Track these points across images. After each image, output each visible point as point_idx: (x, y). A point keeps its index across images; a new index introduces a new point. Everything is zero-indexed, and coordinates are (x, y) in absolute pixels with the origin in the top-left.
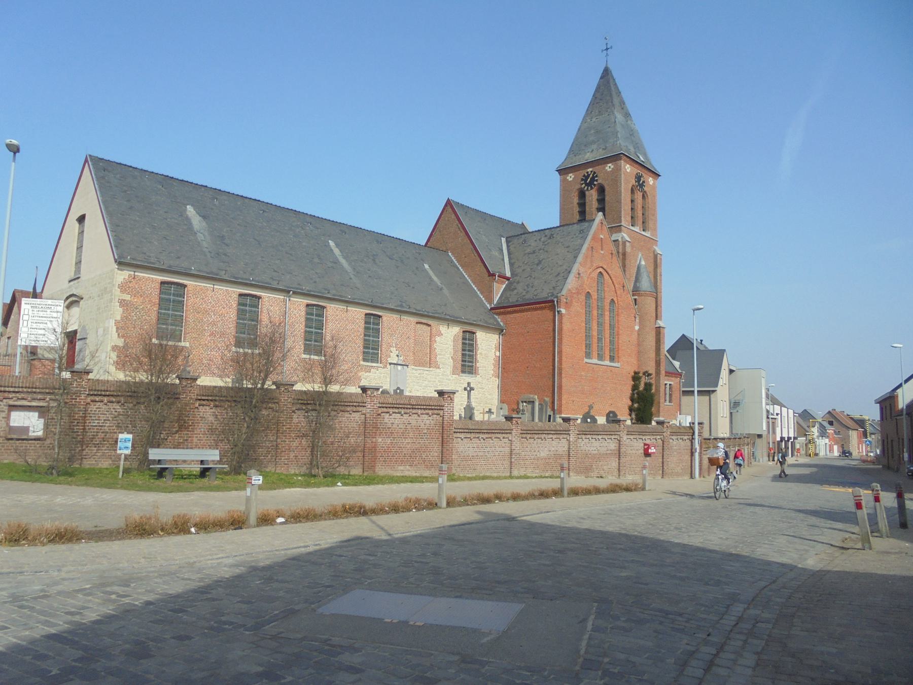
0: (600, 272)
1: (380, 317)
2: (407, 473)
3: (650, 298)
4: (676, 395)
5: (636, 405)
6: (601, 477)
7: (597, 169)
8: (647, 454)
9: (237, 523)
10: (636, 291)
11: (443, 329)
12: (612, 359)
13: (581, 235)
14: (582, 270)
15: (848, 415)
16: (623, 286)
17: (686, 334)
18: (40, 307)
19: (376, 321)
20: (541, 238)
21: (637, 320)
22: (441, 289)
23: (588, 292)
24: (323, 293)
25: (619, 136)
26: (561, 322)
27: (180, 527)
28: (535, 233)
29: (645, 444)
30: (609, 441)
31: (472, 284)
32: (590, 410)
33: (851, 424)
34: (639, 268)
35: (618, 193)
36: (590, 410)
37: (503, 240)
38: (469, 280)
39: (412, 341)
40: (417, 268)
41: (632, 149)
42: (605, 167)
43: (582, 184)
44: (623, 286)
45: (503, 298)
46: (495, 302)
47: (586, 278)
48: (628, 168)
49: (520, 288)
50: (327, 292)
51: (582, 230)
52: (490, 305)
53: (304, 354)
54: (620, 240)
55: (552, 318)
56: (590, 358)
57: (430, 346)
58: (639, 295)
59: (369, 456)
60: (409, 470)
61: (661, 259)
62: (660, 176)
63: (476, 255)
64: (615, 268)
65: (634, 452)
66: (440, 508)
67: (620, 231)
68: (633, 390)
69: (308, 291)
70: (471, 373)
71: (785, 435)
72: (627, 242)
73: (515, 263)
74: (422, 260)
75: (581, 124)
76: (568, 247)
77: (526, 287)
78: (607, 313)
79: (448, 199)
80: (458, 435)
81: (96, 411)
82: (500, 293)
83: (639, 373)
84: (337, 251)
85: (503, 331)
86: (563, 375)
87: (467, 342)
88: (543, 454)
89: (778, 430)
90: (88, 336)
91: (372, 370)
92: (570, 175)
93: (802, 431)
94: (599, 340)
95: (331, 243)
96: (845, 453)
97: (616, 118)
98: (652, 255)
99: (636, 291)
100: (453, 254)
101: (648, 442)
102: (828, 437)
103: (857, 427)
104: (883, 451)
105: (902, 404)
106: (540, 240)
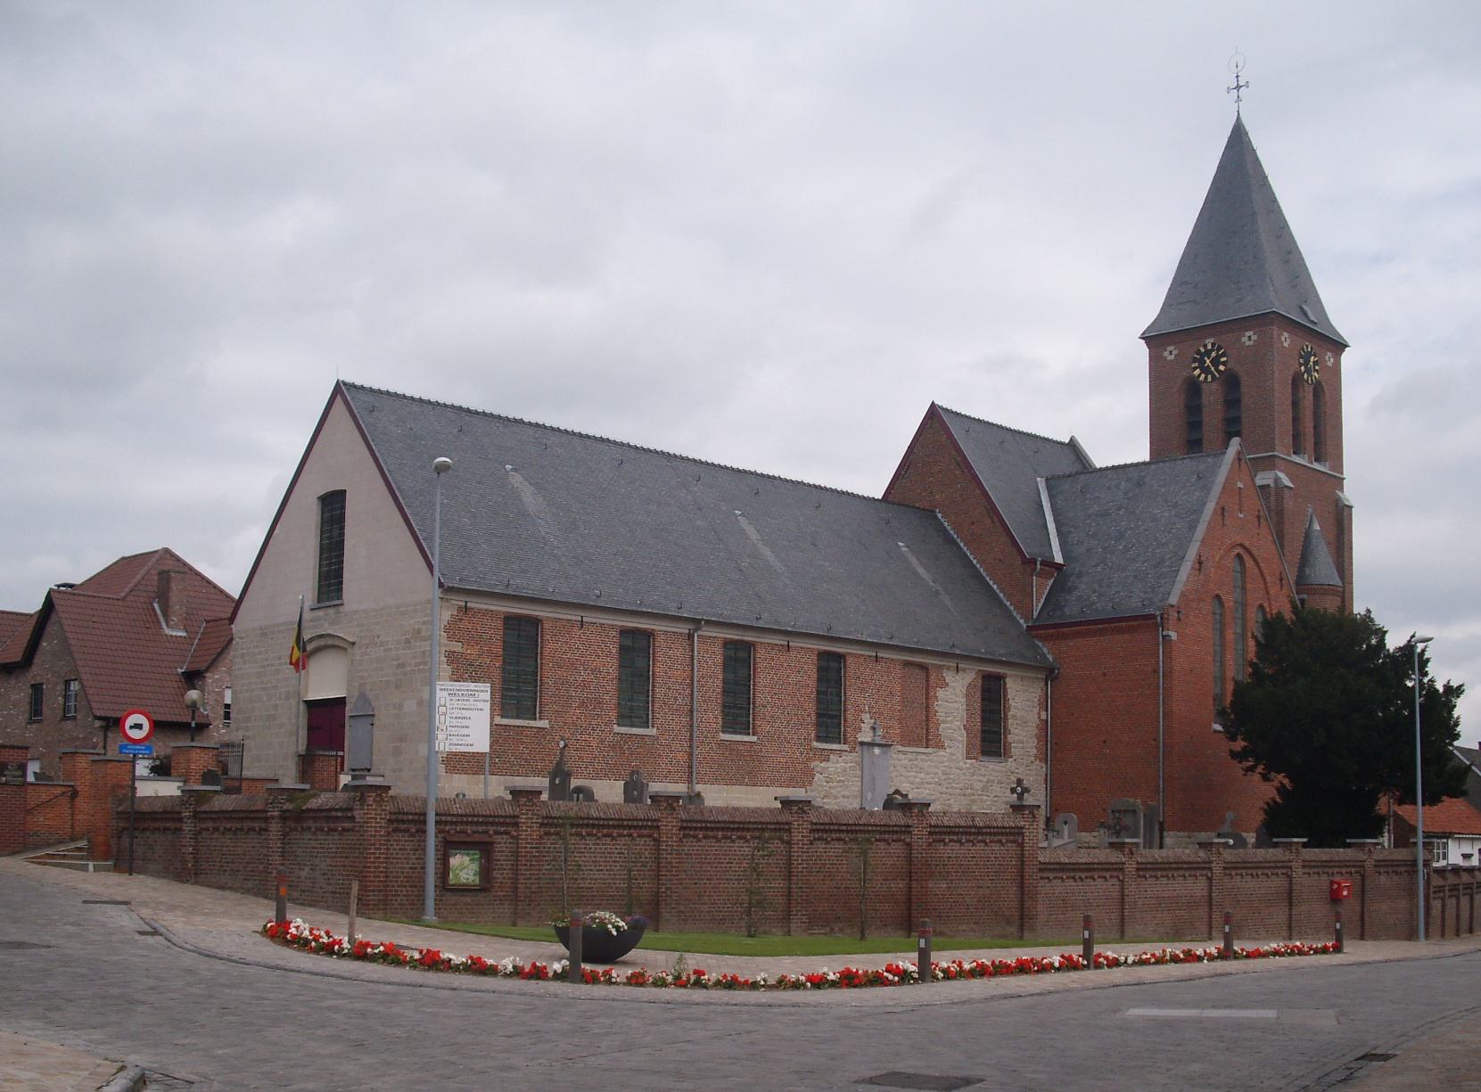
3: (1330, 597)
16: (1281, 580)
18: (460, 693)
20: (1119, 484)
30: (1273, 878)
34: (1308, 535)
42: (1239, 340)
43: (1195, 368)
44: (1281, 580)
53: (723, 732)
57: (927, 707)
64: (1264, 546)
72: (1286, 490)
79: (933, 403)
81: (550, 848)
82: (1044, 597)
85: (1053, 672)
90: (376, 712)
91: (832, 756)
92: (1171, 348)
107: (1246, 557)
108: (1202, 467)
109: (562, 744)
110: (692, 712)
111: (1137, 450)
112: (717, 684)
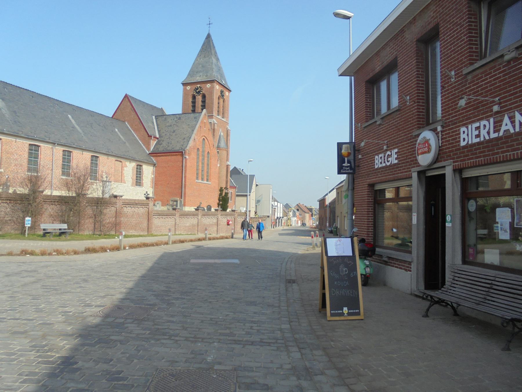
0: (204, 139)
1: (98, 157)
2: (133, 234)
4: (234, 196)
5: (221, 203)
6: (210, 234)
7: (202, 86)
8: (228, 224)
9: (118, 249)
10: (218, 147)
11: (128, 163)
12: (207, 180)
13: (195, 120)
14: (196, 137)
15: (305, 206)
17: (236, 166)
19: (96, 159)
21: (219, 162)
22: (125, 143)
23: (198, 148)
24: (71, 145)
25: (214, 71)
26: (186, 163)
27: (103, 250)
28: (172, 116)
29: (228, 220)
30: (213, 219)
31: (139, 140)
32: (200, 204)
33: (306, 210)
35: (212, 99)
36: (200, 204)
37: (154, 117)
38: (137, 138)
39: (113, 169)
40: (112, 131)
41: (219, 78)
42: (206, 86)
45: (155, 148)
46: (151, 150)
47: (197, 141)
48: (217, 87)
49: (164, 144)
50: (73, 144)
51: (196, 117)
52: (149, 152)
54: (212, 122)
55: (181, 160)
56: (198, 180)
57: (122, 172)
58: (220, 149)
59: (116, 226)
60: (134, 232)
61: (230, 132)
62: (231, 91)
63: (141, 125)
64: (210, 137)
65: (223, 223)
66: (170, 244)
67: (212, 118)
68: (220, 196)
69: (64, 143)
70: (140, 185)
71: (279, 216)
73: (161, 130)
74: (114, 126)
75: (195, 61)
76: (189, 125)
77: (167, 144)
78: (206, 158)
80: (154, 216)
82: (154, 146)
83: (222, 188)
84: (73, 121)
86: (187, 188)
87: (138, 170)
88: (188, 225)
89: (276, 213)
92: (188, 87)
93: (285, 214)
94: (202, 171)
95: (70, 116)
96: (304, 224)
97: (213, 61)
98: (226, 130)
99: (218, 147)
100: (128, 123)
101: (229, 219)
102: (296, 217)
103: (309, 212)
104: (319, 223)
105: (327, 202)
106: (174, 119)
107: (206, 139)
108: (196, 116)
109: (7, 177)
110: (52, 170)
111: (179, 110)
112: (60, 162)
